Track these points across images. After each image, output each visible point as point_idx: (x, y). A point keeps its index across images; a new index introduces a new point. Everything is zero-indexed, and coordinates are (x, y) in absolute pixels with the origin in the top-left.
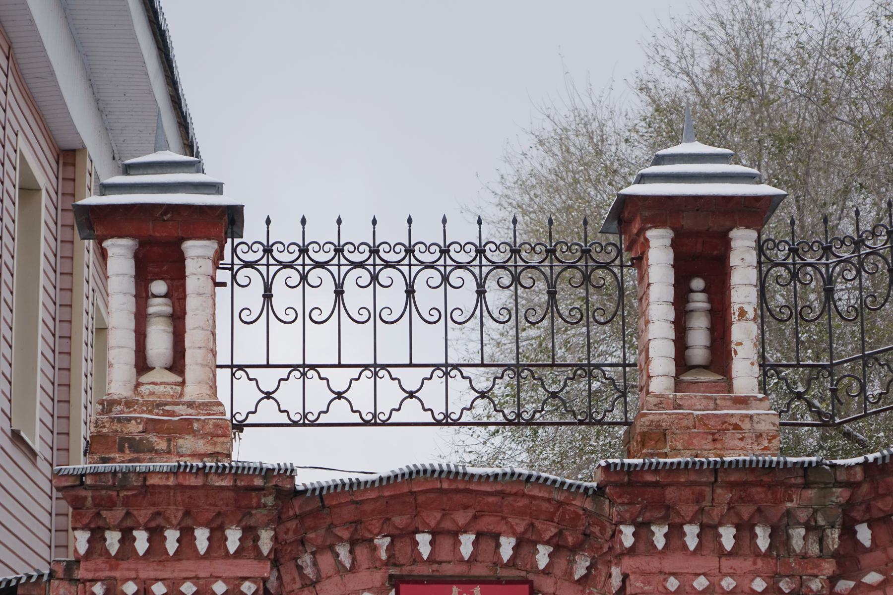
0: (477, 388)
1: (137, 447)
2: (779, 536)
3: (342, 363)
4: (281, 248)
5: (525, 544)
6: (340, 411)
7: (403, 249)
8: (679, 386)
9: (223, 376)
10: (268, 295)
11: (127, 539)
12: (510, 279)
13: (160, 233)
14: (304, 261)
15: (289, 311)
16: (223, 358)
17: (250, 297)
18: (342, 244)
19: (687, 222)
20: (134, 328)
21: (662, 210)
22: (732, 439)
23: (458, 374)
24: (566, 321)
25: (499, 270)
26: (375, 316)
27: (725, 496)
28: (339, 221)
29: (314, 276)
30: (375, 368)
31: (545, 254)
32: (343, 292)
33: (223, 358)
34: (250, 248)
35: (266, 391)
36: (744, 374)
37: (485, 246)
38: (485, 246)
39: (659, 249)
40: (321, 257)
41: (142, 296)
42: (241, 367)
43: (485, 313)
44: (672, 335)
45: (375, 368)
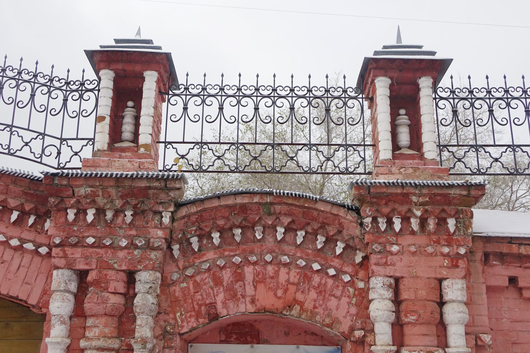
0: (493, 156)
3: (78, 137)
4: (316, 89)
7: (503, 90)
9: (162, 146)
10: (185, 109)
11: (390, 223)
12: (307, 103)
13: (129, 68)
14: (204, 94)
15: (232, 118)
16: (162, 139)
17: (177, 110)
18: (346, 87)
20: (390, 130)
23: (483, 151)
24: (298, 121)
25: (317, 100)
28: (310, 77)
29: (244, 101)
31: (342, 92)
32: (187, 108)
33: (162, 139)
34: (497, 90)
35: (181, 154)
37: (224, 87)
38: (224, 87)
41: (394, 115)
42: (170, 143)
43: (294, 117)
44: (133, 122)
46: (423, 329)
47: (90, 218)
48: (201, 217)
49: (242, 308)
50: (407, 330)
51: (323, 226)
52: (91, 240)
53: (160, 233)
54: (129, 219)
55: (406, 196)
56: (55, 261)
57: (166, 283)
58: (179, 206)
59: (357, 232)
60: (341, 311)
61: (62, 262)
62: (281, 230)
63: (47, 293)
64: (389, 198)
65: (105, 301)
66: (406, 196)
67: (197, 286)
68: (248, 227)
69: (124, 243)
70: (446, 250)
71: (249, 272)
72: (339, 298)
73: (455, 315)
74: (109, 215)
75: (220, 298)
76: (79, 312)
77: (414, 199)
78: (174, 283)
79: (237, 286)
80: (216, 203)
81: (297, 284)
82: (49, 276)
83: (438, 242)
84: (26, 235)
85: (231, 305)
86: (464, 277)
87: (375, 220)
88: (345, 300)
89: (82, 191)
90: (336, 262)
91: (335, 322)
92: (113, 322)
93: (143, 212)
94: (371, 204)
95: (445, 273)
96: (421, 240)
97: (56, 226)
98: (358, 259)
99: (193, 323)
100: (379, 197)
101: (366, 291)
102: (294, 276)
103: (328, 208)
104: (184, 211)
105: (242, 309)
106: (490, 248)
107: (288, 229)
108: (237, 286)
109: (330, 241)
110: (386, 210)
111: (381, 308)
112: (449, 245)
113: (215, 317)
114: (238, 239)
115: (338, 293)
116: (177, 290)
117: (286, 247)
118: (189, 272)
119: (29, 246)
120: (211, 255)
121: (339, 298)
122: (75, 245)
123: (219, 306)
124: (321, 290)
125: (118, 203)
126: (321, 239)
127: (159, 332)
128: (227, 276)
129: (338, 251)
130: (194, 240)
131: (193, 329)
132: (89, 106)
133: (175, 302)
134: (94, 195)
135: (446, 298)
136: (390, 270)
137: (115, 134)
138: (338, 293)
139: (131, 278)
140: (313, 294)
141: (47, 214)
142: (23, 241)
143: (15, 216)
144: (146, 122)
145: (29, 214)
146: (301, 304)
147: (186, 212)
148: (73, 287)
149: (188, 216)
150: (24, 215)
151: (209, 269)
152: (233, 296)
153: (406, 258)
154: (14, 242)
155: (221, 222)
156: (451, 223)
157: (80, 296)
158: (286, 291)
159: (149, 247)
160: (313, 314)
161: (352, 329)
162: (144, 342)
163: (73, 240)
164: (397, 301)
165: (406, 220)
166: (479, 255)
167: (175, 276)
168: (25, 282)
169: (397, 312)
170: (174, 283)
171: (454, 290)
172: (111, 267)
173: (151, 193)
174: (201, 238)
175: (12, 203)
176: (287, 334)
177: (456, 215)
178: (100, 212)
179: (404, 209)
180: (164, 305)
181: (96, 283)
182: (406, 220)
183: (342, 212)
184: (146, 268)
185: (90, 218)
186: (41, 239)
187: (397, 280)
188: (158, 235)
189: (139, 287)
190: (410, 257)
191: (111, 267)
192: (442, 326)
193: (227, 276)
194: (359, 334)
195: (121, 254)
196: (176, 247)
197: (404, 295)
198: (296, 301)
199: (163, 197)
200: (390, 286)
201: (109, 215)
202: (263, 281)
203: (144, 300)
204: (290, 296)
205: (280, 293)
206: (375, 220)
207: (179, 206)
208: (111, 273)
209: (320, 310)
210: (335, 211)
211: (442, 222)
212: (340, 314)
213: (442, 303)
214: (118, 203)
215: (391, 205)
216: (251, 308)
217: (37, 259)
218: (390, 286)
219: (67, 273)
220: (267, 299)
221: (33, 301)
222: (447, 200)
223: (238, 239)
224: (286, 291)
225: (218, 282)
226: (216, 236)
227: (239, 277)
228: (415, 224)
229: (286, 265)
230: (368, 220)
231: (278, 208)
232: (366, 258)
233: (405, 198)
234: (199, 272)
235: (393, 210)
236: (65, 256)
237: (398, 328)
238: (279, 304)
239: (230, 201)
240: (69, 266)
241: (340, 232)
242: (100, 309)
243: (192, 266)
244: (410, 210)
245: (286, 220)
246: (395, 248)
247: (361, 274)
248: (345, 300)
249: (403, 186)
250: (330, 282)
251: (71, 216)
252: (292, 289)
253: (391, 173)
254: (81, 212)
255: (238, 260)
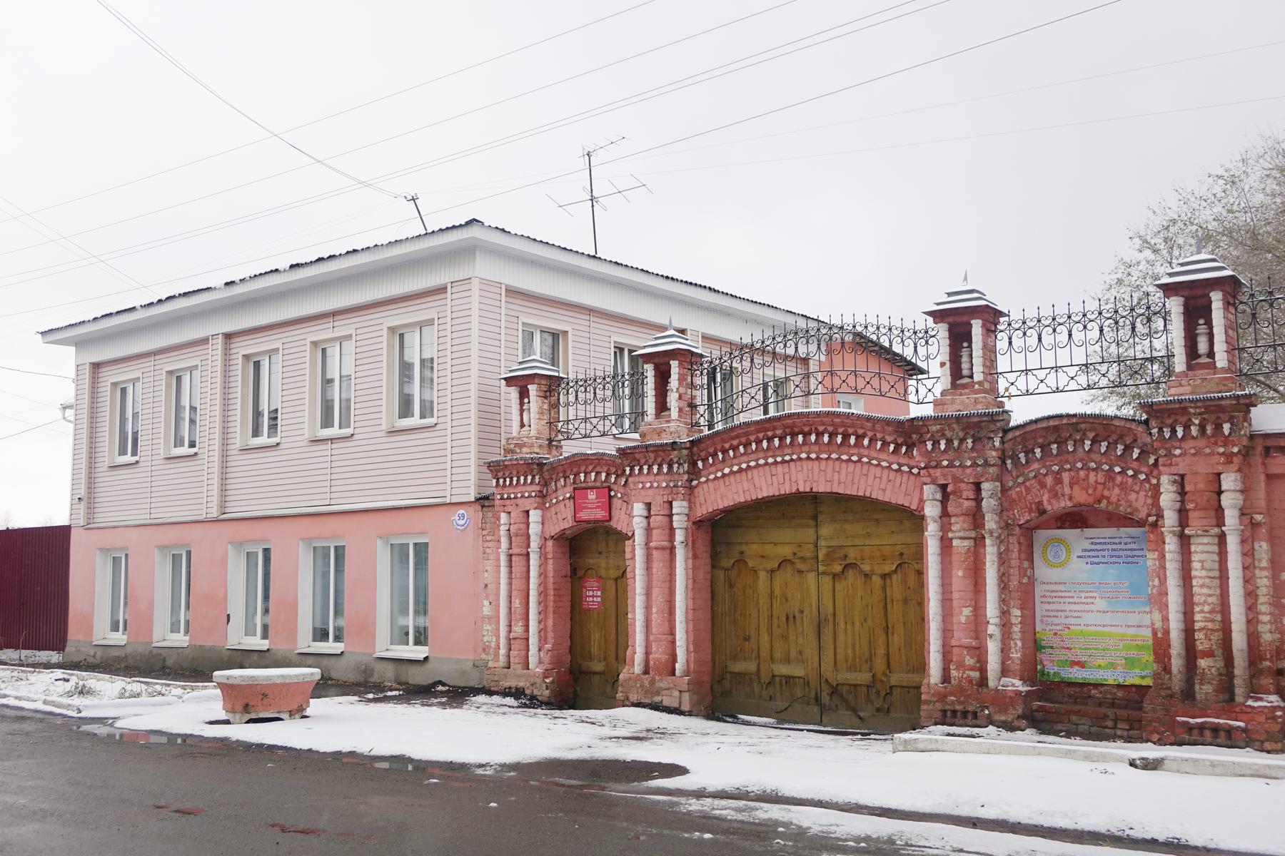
1: (513, 452)
2: (670, 467)
5: (608, 475)
6: (1043, 388)
8: (1190, 367)
11: (1174, 431)
13: (958, 319)
19: (656, 361)
21: (648, 358)
22: (663, 435)
26: (1025, 349)
27: (652, 455)
30: (1056, 368)
36: (674, 413)
39: (649, 371)
40: (1062, 321)
45: (1056, 368)
46: (1202, 514)
47: (943, 447)
48: (1024, 438)
49: (1063, 504)
50: (1191, 515)
51: (1121, 437)
52: (945, 463)
53: (994, 453)
54: (970, 445)
55: (1185, 409)
56: (924, 479)
57: (1004, 490)
58: (1006, 431)
59: (1148, 440)
60: (1140, 502)
61: (928, 480)
62: (1088, 443)
63: (921, 501)
64: (1171, 412)
65: (961, 505)
66: (1185, 409)
67: (1028, 489)
68: (1061, 443)
69: (969, 463)
70: (1222, 450)
71: (1066, 476)
72: (1138, 493)
73: (1230, 502)
74: (956, 443)
75: (1046, 497)
76: (945, 514)
77: (1192, 411)
78: (1010, 488)
79: (1058, 488)
80: (1034, 427)
81: (1104, 484)
82: (922, 489)
83: (1216, 444)
84: (902, 461)
85: (1054, 502)
86: (1239, 470)
87: (1161, 430)
88: (1142, 494)
89: (934, 428)
90: (1135, 465)
91: (1136, 510)
92: (970, 519)
93: (980, 439)
94: (1157, 418)
95: (1220, 468)
96: (1201, 443)
97: (921, 454)
98: (1151, 461)
99: (1027, 517)
100: (1162, 411)
101: (1158, 485)
102: (1101, 478)
103: (1122, 423)
104: (1010, 435)
105: (1064, 504)
106: (1269, 443)
107: (1094, 441)
108: (1058, 488)
109: (1128, 448)
110: (1169, 421)
111: (1168, 499)
112: (1225, 445)
113: (1042, 512)
114: (1055, 452)
115: (1137, 488)
116: (1013, 493)
117: (1093, 456)
118: (1020, 480)
119: (905, 469)
120: (1035, 466)
121: (1138, 493)
122: (936, 467)
123: (1045, 503)
124: (1123, 487)
125: (961, 434)
126: (1120, 447)
127: (1003, 524)
128: (1049, 480)
129: (1135, 456)
130: (1022, 455)
131: (1027, 522)
132: (933, 350)
133: (1013, 503)
134: (942, 430)
135: (1223, 488)
136: (1174, 470)
137: (956, 372)
138: (1137, 488)
139: (978, 487)
140: (1117, 490)
141: (914, 445)
142: (900, 465)
143: (892, 447)
144: (978, 362)
145: (902, 445)
146: (1108, 498)
147: (661, 681)
148: (939, 496)
149: (1015, 438)
150: (898, 447)
151: (1035, 477)
152: (1055, 495)
153: (1188, 459)
154: (895, 467)
155: (1040, 441)
156: (1226, 428)
157: (944, 501)
158: (1095, 489)
159: (986, 464)
160: (1118, 506)
161: (1149, 515)
162: (991, 533)
163: (933, 464)
164: (1182, 493)
165: (1187, 428)
166: (1259, 449)
167: (1011, 484)
168: (906, 494)
169: (1182, 502)
170: (1010, 488)
171: (1229, 481)
172: (962, 481)
173: (987, 424)
174: (1027, 453)
175: (889, 439)
176: (1109, 520)
177: (1231, 420)
178: (949, 442)
179: (1184, 419)
180: (1005, 505)
181: (954, 492)
182: (1187, 428)
183: (1134, 426)
184: (987, 480)
185: (943, 447)
186: (912, 463)
187: (1182, 476)
188: (993, 455)
189: (984, 494)
190: (1191, 457)
191: (962, 481)
192: (1219, 510)
193: (1049, 480)
194: (1152, 519)
195: (968, 471)
196: (1009, 462)
197: (1187, 489)
198: (1103, 497)
199: (992, 427)
200: (1175, 482)
201: (956, 443)
202: (1077, 483)
203: (988, 504)
204: (1098, 493)
205: (1090, 491)
206: (1161, 430)
207: (1006, 431)
208: (963, 486)
209: (1123, 502)
210: (1128, 425)
211: (1218, 427)
212: (1139, 504)
213: (1220, 493)
214: (961, 434)
215: (1173, 417)
216: (1069, 504)
217: (912, 477)
218: (1175, 482)
219: (933, 487)
220: (1081, 496)
221: (914, 507)
222: (1221, 409)
223: (1055, 452)
224: (1095, 489)
225: (1043, 485)
226: (1038, 451)
227: (1059, 481)
228: (1194, 431)
229: (1094, 470)
230: (1155, 431)
231: (1083, 426)
232: (1156, 460)
233: (1184, 410)
234: (1027, 479)
235: (1176, 421)
236: (930, 475)
237: (1183, 513)
238: (1091, 500)
239: (1045, 425)
240: (933, 482)
241: (1135, 441)
242: (958, 511)
243: (1022, 475)
244: (1190, 420)
245: (1091, 435)
246: (1178, 452)
247: (1155, 473)
248: (1142, 494)
249: (1180, 402)
250: (1130, 480)
251: (929, 447)
252: (1100, 487)
253: (1181, 385)
254: (936, 443)
255: (1056, 468)
